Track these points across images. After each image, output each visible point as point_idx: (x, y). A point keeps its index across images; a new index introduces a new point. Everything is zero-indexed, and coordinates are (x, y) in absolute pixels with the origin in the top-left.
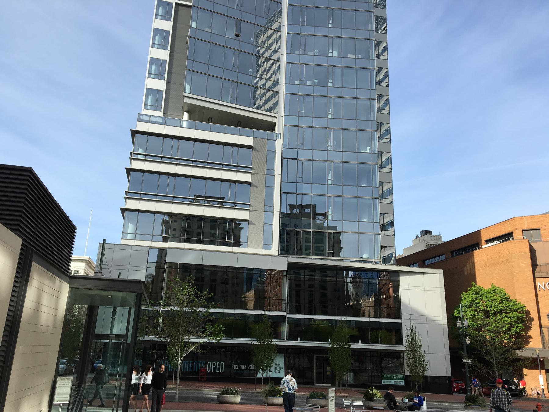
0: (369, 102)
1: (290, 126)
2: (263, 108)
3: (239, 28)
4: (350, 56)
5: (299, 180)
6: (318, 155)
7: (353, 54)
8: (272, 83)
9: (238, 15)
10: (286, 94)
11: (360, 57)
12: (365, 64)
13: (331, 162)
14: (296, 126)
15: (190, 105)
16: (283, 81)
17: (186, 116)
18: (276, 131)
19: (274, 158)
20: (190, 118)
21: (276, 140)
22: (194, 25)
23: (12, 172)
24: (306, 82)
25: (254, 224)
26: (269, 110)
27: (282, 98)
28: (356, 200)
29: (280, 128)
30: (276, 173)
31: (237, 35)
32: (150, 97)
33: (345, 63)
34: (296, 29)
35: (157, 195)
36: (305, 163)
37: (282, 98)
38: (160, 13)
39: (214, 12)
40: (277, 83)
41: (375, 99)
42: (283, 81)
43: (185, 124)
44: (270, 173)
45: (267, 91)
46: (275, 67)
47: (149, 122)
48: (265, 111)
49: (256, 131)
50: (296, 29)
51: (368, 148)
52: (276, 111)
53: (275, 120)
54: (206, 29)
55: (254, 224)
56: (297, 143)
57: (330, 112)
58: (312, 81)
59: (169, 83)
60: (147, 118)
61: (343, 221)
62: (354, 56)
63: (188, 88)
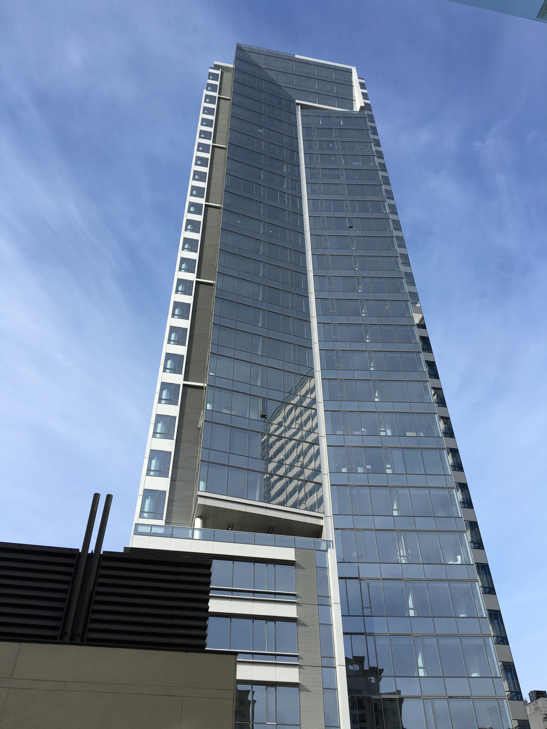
0: (446, 492)
1: (342, 529)
2: (303, 506)
3: (264, 408)
4: (408, 434)
5: (367, 612)
6: (387, 571)
7: (412, 431)
8: (310, 472)
9: (263, 393)
10: (332, 485)
11: (422, 435)
12: (431, 443)
13: (408, 580)
14: (352, 529)
15: (205, 507)
16: (325, 469)
17: (198, 523)
18: (324, 536)
19: (326, 579)
20: (204, 525)
21: (327, 551)
22: (209, 407)
23: (181, 569)
24: (356, 470)
25: (308, 691)
26: (312, 508)
27: (327, 491)
28: (457, 641)
29: (329, 533)
30: (333, 602)
31: (263, 416)
32: (148, 502)
33: (404, 443)
34: (335, 406)
35: (253, 654)
36: (373, 584)
37: (327, 491)
38: (164, 397)
39: (234, 391)
40: (317, 471)
41: (453, 488)
42: (325, 469)
43: (197, 535)
44: (324, 602)
45: (305, 482)
46: (312, 451)
47: (150, 534)
48: (306, 509)
49: (297, 538)
50: (335, 406)
51: (459, 557)
52: (321, 509)
53: (321, 522)
54: (225, 411)
55: (308, 691)
56: (355, 554)
57: (395, 507)
58: (364, 467)
59: (173, 480)
60: (147, 530)
61: (443, 677)
62: (414, 434)
63: (202, 485)
